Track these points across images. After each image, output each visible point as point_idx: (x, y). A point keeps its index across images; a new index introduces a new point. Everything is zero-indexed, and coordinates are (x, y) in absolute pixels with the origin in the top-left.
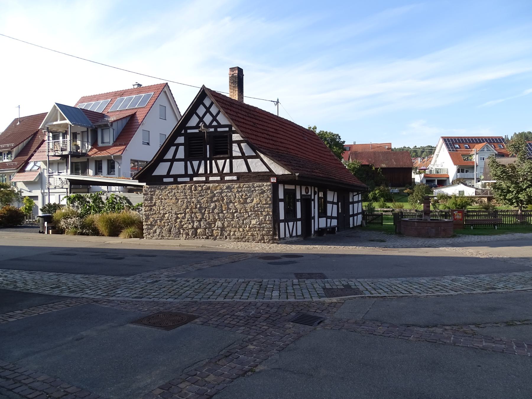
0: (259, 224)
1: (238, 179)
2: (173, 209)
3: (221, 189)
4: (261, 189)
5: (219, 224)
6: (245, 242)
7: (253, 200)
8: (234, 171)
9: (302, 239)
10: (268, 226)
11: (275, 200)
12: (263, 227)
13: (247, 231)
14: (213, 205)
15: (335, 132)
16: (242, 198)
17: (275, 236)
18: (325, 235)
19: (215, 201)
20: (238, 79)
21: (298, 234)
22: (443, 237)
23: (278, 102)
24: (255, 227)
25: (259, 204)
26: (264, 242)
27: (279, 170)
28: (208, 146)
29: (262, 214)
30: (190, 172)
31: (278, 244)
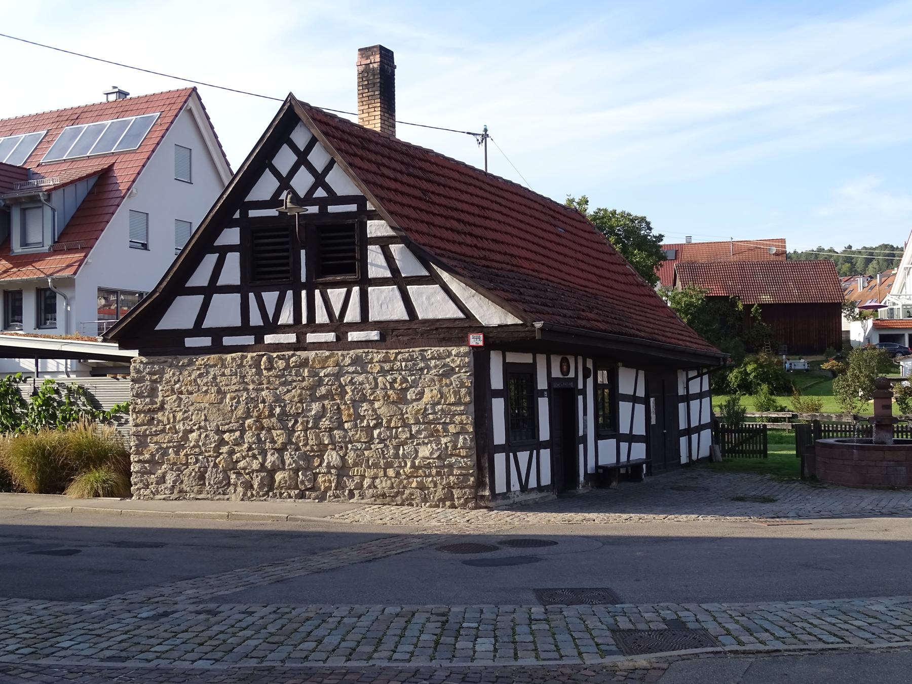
0: (439, 457)
1: (383, 337)
3: (337, 365)
4: (444, 365)
7: (422, 394)
9: (552, 496)
10: (464, 461)
11: (481, 394)
12: (451, 466)
14: (315, 407)
15: (636, 212)
16: (392, 388)
21: (543, 483)
23: (485, 136)
25: (438, 403)
26: (453, 506)
28: (303, 252)
29: (445, 430)
30: (256, 320)
31: (490, 509)
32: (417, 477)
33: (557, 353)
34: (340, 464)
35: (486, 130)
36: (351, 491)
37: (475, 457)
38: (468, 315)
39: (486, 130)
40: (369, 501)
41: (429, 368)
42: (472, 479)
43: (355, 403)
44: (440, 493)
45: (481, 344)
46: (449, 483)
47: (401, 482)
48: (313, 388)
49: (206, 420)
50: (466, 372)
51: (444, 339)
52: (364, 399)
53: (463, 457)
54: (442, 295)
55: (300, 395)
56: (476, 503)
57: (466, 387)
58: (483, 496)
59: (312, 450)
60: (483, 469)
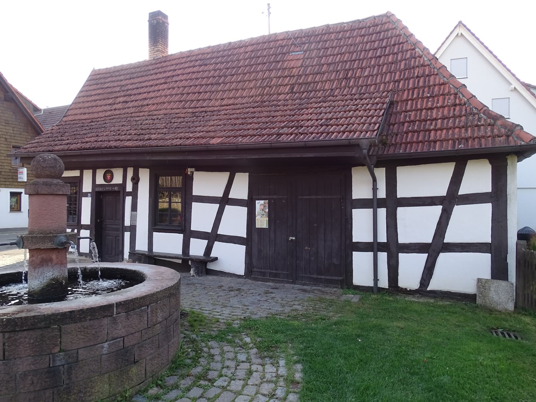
20: (158, 28)
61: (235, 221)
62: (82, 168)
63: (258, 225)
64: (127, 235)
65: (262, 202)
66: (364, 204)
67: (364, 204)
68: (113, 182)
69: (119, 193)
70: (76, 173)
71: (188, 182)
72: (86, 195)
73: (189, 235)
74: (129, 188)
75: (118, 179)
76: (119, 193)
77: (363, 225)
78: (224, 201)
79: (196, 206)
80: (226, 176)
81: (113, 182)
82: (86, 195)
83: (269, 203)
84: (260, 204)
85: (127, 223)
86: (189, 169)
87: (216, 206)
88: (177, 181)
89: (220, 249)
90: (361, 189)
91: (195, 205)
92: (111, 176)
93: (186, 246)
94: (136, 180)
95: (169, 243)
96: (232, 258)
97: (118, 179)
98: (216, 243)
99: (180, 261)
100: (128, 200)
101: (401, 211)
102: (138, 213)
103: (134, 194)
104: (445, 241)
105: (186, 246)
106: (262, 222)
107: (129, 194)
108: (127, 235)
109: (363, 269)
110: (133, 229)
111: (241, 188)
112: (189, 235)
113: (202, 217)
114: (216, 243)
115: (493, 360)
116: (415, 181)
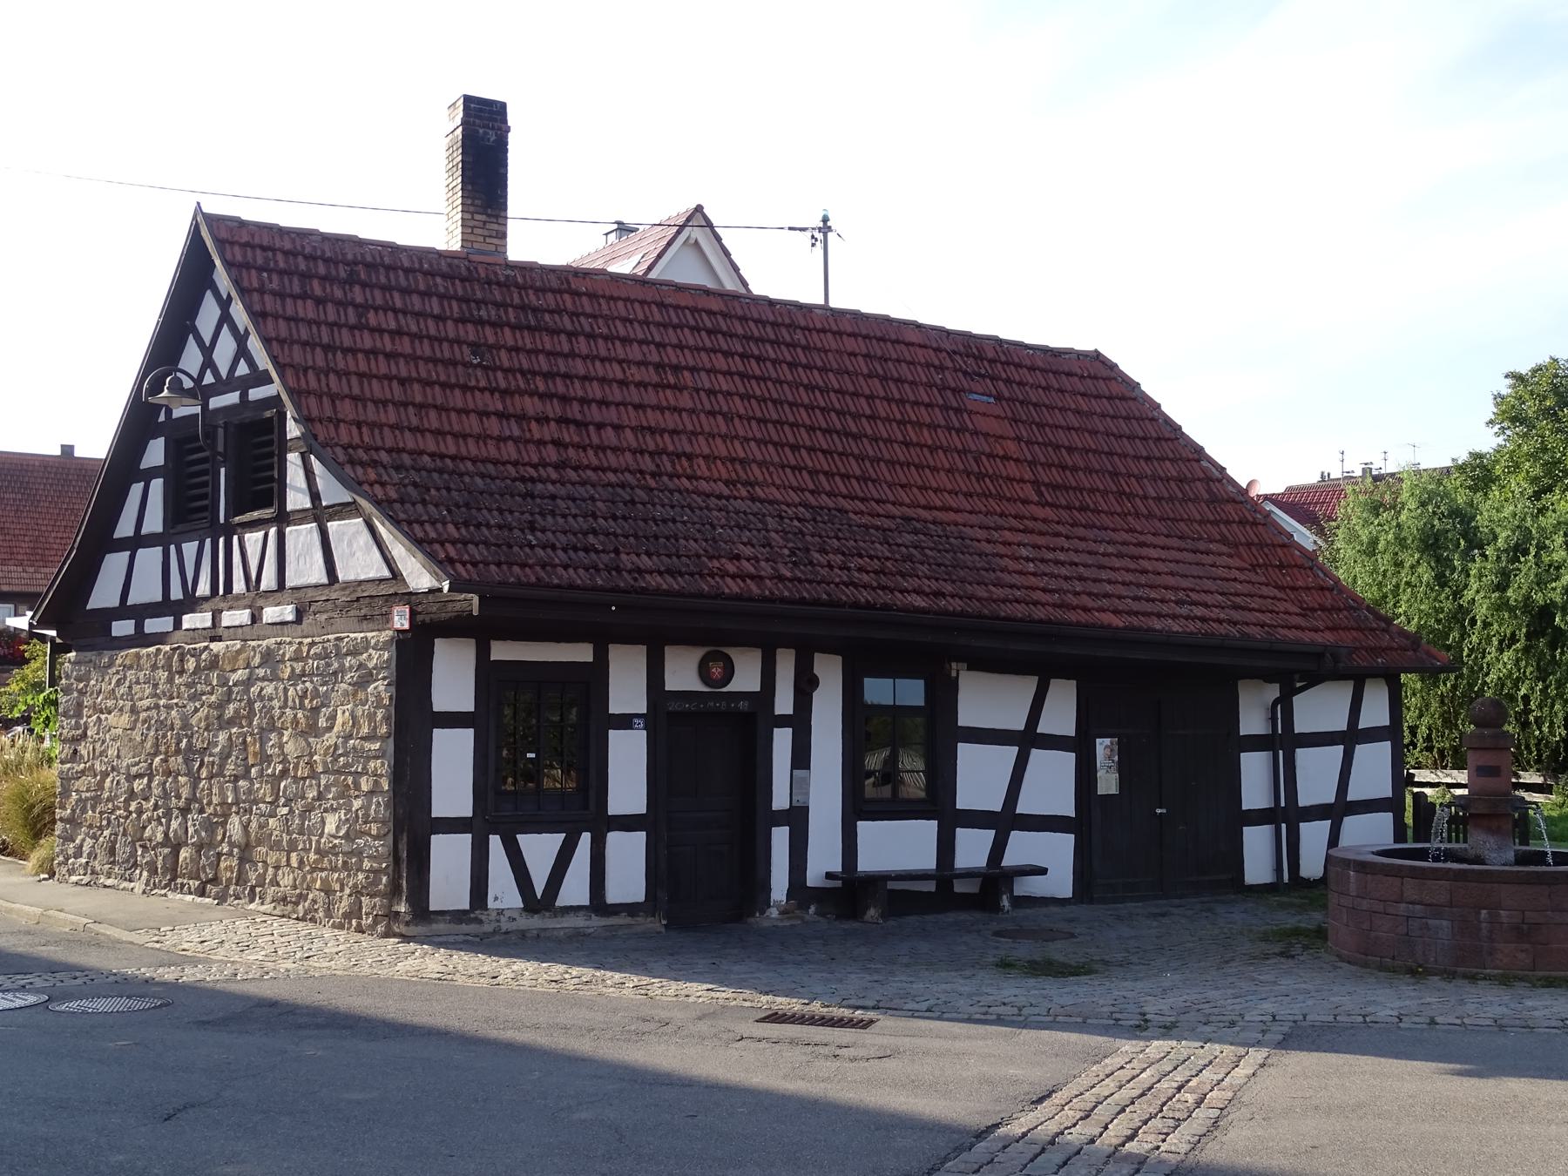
0: (347, 836)
1: (300, 614)
2: (122, 753)
3: (248, 666)
4: (361, 666)
5: (235, 826)
6: (303, 919)
7: (333, 718)
8: (290, 582)
9: (655, 924)
10: (375, 847)
11: (413, 721)
12: (359, 853)
13: (313, 870)
14: (222, 737)
15: (1543, 359)
16: (302, 707)
17: (407, 904)
18: (872, 913)
19: (231, 722)
20: (483, 141)
21: (613, 895)
22: (1505, 981)
23: (825, 228)
24: (333, 850)
25: (350, 736)
26: (360, 930)
27: (419, 576)
28: (223, 470)
29: (357, 786)
30: (176, 593)
31: (406, 939)
32: (322, 870)
33: (686, 639)
34: (243, 841)
35: (825, 220)
36: (253, 888)
37: (391, 836)
38: (396, 575)
39: (825, 220)
40: (267, 907)
41: (342, 670)
42: (384, 879)
43: (263, 733)
44: (344, 906)
45: (407, 626)
46: (355, 886)
47: (304, 878)
48: (221, 706)
49: (118, 757)
50: (384, 679)
51: (365, 618)
52: (273, 728)
53: (375, 838)
54: (365, 536)
55: (207, 718)
56: (388, 927)
57: (384, 706)
58: (398, 913)
59: (215, 815)
60: (411, 863)
61: (1051, 784)
62: (601, 641)
63: (1102, 789)
64: (780, 837)
65: (1107, 741)
66: (1256, 743)
67: (1256, 743)
68: (733, 687)
69: (752, 719)
70: (582, 653)
71: (943, 698)
72: (625, 722)
73: (950, 819)
74: (784, 703)
75: (746, 679)
76: (752, 719)
77: (1255, 780)
78: (1028, 739)
79: (967, 753)
80: (1029, 685)
81: (733, 687)
82: (625, 722)
83: (1119, 743)
84: (1102, 746)
85: (780, 801)
86: (954, 665)
87: (1012, 751)
88: (912, 692)
89: (1022, 848)
90: (1252, 722)
91: (965, 750)
92: (724, 668)
93: (946, 847)
94: (805, 686)
95: (898, 847)
96: (1050, 861)
97: (746, 679)
98: (1015, 835)
99: (930, 886)
100: (782, 740)
101: (1301, 753)
102: (812, 777)
103: (800, 723)
104: (1349, 799)
105: (946, 847)
106: (1107, 783)
107: (783, 721)
108: (780, 837)
109: (1257, 846)
110: (797, 818)
111: (1060, 716)
112: (950, 819)
113: (980, 777)
114: (1015, 835)
115: (1526, 699)
116: (1321, 708)
